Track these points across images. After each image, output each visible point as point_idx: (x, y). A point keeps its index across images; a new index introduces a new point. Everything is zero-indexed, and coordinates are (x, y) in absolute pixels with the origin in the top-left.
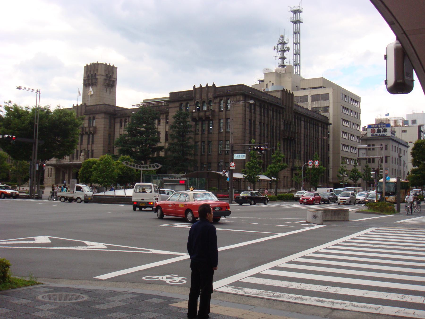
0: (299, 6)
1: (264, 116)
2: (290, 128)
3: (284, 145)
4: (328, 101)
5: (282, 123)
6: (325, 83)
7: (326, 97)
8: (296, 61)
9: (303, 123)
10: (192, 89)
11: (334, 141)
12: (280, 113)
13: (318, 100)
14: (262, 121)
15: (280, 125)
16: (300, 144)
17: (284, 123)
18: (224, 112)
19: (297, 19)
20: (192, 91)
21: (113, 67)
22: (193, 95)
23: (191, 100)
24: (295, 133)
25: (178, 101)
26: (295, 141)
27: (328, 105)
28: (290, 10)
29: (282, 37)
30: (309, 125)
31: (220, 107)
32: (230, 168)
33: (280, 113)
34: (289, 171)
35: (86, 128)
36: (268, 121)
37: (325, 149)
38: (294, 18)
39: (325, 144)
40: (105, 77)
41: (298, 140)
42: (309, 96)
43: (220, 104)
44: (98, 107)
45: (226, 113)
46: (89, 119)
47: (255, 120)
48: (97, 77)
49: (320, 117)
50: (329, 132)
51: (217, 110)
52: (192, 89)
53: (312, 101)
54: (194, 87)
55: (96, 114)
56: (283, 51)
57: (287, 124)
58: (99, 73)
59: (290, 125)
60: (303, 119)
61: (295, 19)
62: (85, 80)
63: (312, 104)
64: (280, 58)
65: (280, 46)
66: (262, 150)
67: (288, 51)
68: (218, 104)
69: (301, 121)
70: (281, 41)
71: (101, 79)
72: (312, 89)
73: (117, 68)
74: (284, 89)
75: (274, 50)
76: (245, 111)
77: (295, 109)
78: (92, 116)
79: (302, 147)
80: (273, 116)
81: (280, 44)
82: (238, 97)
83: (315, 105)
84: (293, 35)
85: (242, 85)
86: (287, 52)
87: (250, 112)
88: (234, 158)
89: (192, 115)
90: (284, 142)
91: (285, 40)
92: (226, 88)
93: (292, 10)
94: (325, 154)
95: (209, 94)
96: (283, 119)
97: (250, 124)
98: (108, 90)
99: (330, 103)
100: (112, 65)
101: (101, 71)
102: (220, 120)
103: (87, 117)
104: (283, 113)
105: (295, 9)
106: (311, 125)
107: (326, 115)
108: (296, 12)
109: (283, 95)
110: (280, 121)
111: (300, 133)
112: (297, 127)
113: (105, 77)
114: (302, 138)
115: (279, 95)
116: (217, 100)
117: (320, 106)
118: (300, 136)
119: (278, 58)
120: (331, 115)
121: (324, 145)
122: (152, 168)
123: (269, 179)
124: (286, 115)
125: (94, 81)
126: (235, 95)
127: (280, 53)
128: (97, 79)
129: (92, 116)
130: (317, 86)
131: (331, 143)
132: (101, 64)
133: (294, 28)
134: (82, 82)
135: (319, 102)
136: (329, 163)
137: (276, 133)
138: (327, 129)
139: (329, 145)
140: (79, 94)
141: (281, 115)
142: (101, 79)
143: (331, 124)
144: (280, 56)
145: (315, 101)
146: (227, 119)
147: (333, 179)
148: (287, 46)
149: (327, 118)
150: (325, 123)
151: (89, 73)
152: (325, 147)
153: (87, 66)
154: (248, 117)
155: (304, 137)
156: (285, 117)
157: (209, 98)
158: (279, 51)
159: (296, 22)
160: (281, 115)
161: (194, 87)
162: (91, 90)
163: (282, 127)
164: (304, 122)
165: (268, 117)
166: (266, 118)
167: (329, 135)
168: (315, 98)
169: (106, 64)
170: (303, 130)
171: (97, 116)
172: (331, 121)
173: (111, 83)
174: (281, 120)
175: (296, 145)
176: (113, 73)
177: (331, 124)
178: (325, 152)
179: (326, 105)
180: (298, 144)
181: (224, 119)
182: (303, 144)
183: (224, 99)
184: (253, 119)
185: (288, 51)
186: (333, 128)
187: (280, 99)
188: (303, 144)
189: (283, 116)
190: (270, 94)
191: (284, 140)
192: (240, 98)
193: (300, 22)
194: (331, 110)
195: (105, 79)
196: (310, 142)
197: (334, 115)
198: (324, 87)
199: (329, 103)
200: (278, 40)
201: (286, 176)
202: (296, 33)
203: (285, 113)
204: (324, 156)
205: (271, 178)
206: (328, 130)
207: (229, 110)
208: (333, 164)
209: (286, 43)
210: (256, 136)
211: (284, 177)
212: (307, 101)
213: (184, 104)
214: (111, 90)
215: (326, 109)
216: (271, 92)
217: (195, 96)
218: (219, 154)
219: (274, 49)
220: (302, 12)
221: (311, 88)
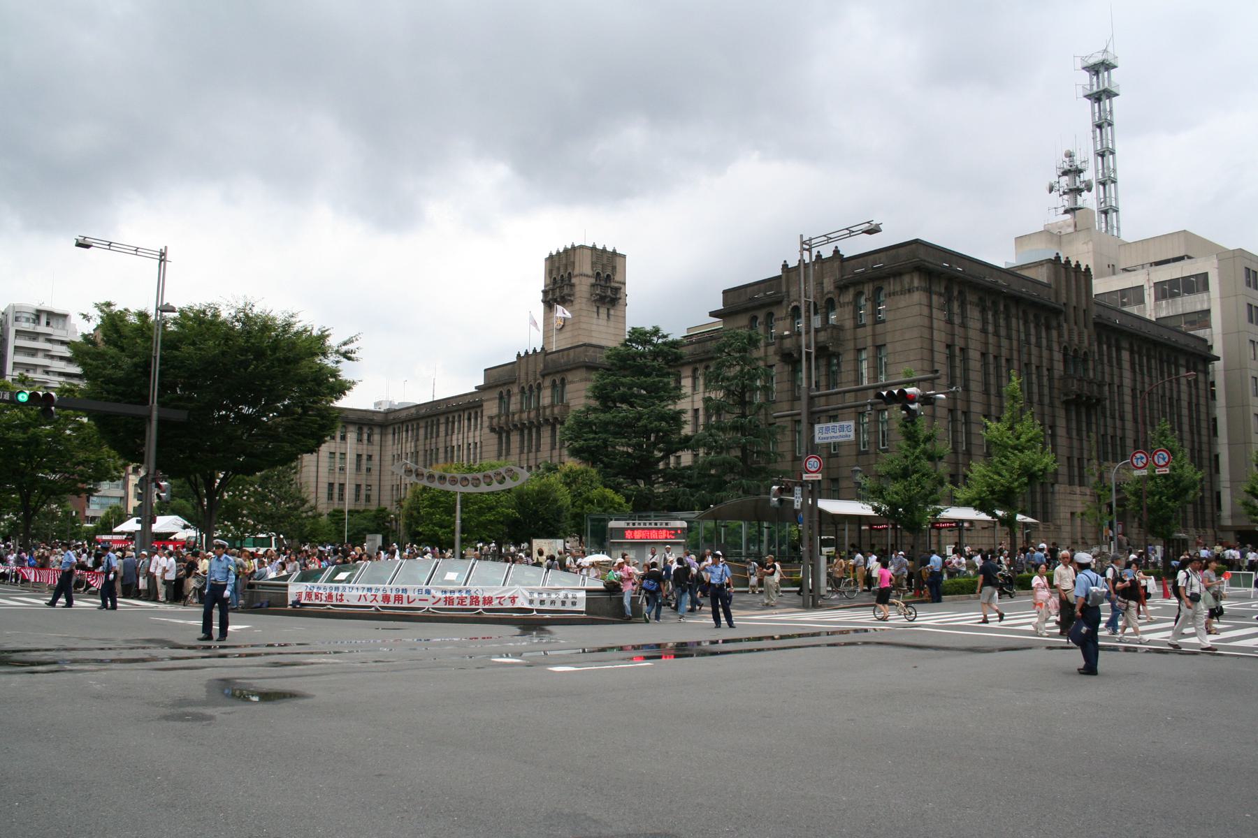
0: (1105, 51)
1: (997, 334)
2: (1086, 370)
3: (1068, 420)
4: (1205, 295)
5: (1058, 356)
6: (1187, 245)
7: (1198, 284)
8: (1105, 201)
9: (1125, 355)
10: (779, 273)
11: (1229, 406)
12: (1048, 328)
13: (1173, 295)
14: (991, 349)
15: (1051, 360)
16: (1122, 419)
17: (1065, 355)
18: (869, 329)
19: (1102, 88)
20: (779, 277)
21: (614, 253)
22: (784, 289)
23: (779, 303)
24: (1100, 385)
25: (746, 310)
26: (1104, 408)
27: (1205, 307)
28: (1079, 65)
29: (1070, 155)
30: (1148, 361)
31: (856, 316)
32: (805, 477)
33: (1048, 328)
34: (1088, 498)
35: (544, 408)
36: (1011, 349)
37: (1204, 432)
38: (1092, 85)
39: (1203, 416)
40: (593, 281)
41: (1112, 402)
42: (1146, 287)
43: (857, 307)
44: (572, 352)
45: (873, 330)
46: (554, 384)
47: (967, 345)
48: (574, 280)
49: (1183, 341)
50: (1213, 384)
51: (849, 324)
52: (779, 273)
53: (1156, 299)
54: (785, 266)
55: (568, 370)
56: (1077, 191)
57: (1074, 358)
58: (576, 272)
59: (1085, 361)
60: (1182, 361)
61: (1095, 89)
62: (545, 292)
63: (1157, 307)
64: (1066, 212)
65: (1065, 180)
66: (912, 399)
67: (1089, 190)
68: (851, 307)
69: (1119, 349)
70: (1067, 167)
71: (583, 286)
72: (1154, 268)
73: (624, 256)
74: (1058, 258)
75: (1051, 190)
76: (931, 317)
77: (1099, 316)
78: (558, 378)
79: (1129, 425)
80: (1028, 334)
81: (1065, 173)
82: (906, 279)
83: (1167, 309)
84: (1094, 131)
85: (917, 242)
86: (1085, 194)
87: (950, 322)
88: (817, 441)
89: (781, 344)
90: (1067, 411)
91: (1078, 163)
92: (871, 257)
93: (1085, 65)
94: (1205, 447)
95: (826, 281)
96: (1060, 343)
97: (951, 357)
98: (603, 311)
99: (1213, 300)
100: (610, 249)
101: (584, 266)
102: (859, 351)
103: (548, 382)
104: (1059, 326)
105: (1092, 61)
106: (1153, 361)
107: (1201, 333)
108: (1099, 68)
109: (1056, 274)
110: (1050, 349)
111: (1120, 386)
112: (1107, 369)
113: (593, 281)
114: (1128, 399)
115: (1042, 275)
116: (848, 296)
117: (1180, 311)
118: (1121, 394)
119: (1063, 209)
120: (1216, 335)
121: (1198, 420)
122: (483, 485)
123: (983, 516)
124: (1070, 331)
125: (566, 291)
126: (897, 274)
127: (1066, 197)
128: (572, 286)
129: (558, 378)
130: (1170, 257)
131: (1221, 413)
132: (582, 247)
133: (1093, 114)
134: (541, 296)
135: (1179, 299)
136: (1217, 471)
137: (1040, 386)
138: (1206, 373)
139: (1215, 420)
140: (535, 324)
141: (1054, 333)
142: (583, 286)
143: (1218, 359)
144: (1068, 205)
145: (1164, 297)
146: (879, 347)
147: (1233, 516)
148: (1085, 176)
149: (1206, 341)
150: (1202, 357)
151: (554, 273)
152: (1204, 424)
153: (551, 256)
154: (940, 337)
155: (1134, 397)
156: (1066, 337)
157: (826, 291)
158: (1065, 193)
159: (1100, 96)
160: (1054, 333)
161: (785, 266)
162: (561, 312)
163: (1059, 367)
164: (1132, 352)
165: (1009, 338)
166: (1004, 342)
167: (1213, 393)
168: (1167, 290)
169: (594, 248)
170: (1127, 374)
171: (569, 377)
172: (1217, 350)
173: (609, 293)
174: (1055, 347)
175: (1109, 420)
176: (614, 268)
177: (1218, 359)
178: (1205, 439)
179: (1199, 308)
180: (1113, 418)
181: (870, 349)
182: (1129, 416)
183: (868, 289)
184: (959, 343)
185: (1089, 190)
186: (1226, 370)
187: (1048, 286)
188: (1129, 416)
189: (1060, 335)
190: (1026, 273)
191: (1067, 404)
192: (912, 281)
193: (1110, 94)
194: (1216, 318)
195: (593, 285)
196: (1151, 410)
197: (1225, 334)
198: (1189, 258)
199: (1209, 299)
200: (1060, 164)
201: (1079, 511)
202: (1100, 126)
203: (1065, 325)
204: (1200, 451)
205: (994, 515)
206: (1211, 379)
207: (884, 321)
208: (1231, 474)
209: (1081, 171)
210: (972, 394)
211: (1072, 514)
212: (1141, 301)
213: (761, 316)
214: (612, 312)
215: (1203, 317)
216: (1022, 267)
217: (788, 292)
218: (860, 453)
219: (1051, 190)
220: (1115, 67)
221: (1151, 265)
